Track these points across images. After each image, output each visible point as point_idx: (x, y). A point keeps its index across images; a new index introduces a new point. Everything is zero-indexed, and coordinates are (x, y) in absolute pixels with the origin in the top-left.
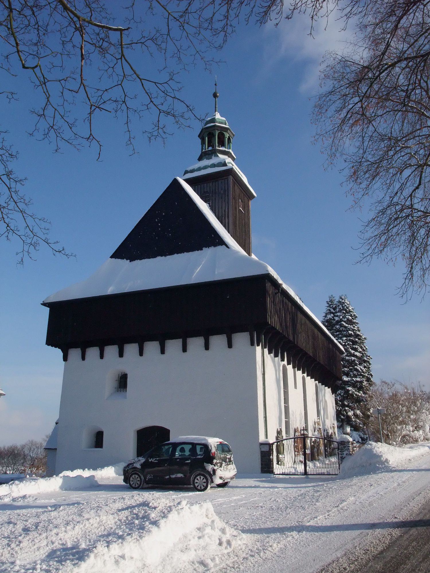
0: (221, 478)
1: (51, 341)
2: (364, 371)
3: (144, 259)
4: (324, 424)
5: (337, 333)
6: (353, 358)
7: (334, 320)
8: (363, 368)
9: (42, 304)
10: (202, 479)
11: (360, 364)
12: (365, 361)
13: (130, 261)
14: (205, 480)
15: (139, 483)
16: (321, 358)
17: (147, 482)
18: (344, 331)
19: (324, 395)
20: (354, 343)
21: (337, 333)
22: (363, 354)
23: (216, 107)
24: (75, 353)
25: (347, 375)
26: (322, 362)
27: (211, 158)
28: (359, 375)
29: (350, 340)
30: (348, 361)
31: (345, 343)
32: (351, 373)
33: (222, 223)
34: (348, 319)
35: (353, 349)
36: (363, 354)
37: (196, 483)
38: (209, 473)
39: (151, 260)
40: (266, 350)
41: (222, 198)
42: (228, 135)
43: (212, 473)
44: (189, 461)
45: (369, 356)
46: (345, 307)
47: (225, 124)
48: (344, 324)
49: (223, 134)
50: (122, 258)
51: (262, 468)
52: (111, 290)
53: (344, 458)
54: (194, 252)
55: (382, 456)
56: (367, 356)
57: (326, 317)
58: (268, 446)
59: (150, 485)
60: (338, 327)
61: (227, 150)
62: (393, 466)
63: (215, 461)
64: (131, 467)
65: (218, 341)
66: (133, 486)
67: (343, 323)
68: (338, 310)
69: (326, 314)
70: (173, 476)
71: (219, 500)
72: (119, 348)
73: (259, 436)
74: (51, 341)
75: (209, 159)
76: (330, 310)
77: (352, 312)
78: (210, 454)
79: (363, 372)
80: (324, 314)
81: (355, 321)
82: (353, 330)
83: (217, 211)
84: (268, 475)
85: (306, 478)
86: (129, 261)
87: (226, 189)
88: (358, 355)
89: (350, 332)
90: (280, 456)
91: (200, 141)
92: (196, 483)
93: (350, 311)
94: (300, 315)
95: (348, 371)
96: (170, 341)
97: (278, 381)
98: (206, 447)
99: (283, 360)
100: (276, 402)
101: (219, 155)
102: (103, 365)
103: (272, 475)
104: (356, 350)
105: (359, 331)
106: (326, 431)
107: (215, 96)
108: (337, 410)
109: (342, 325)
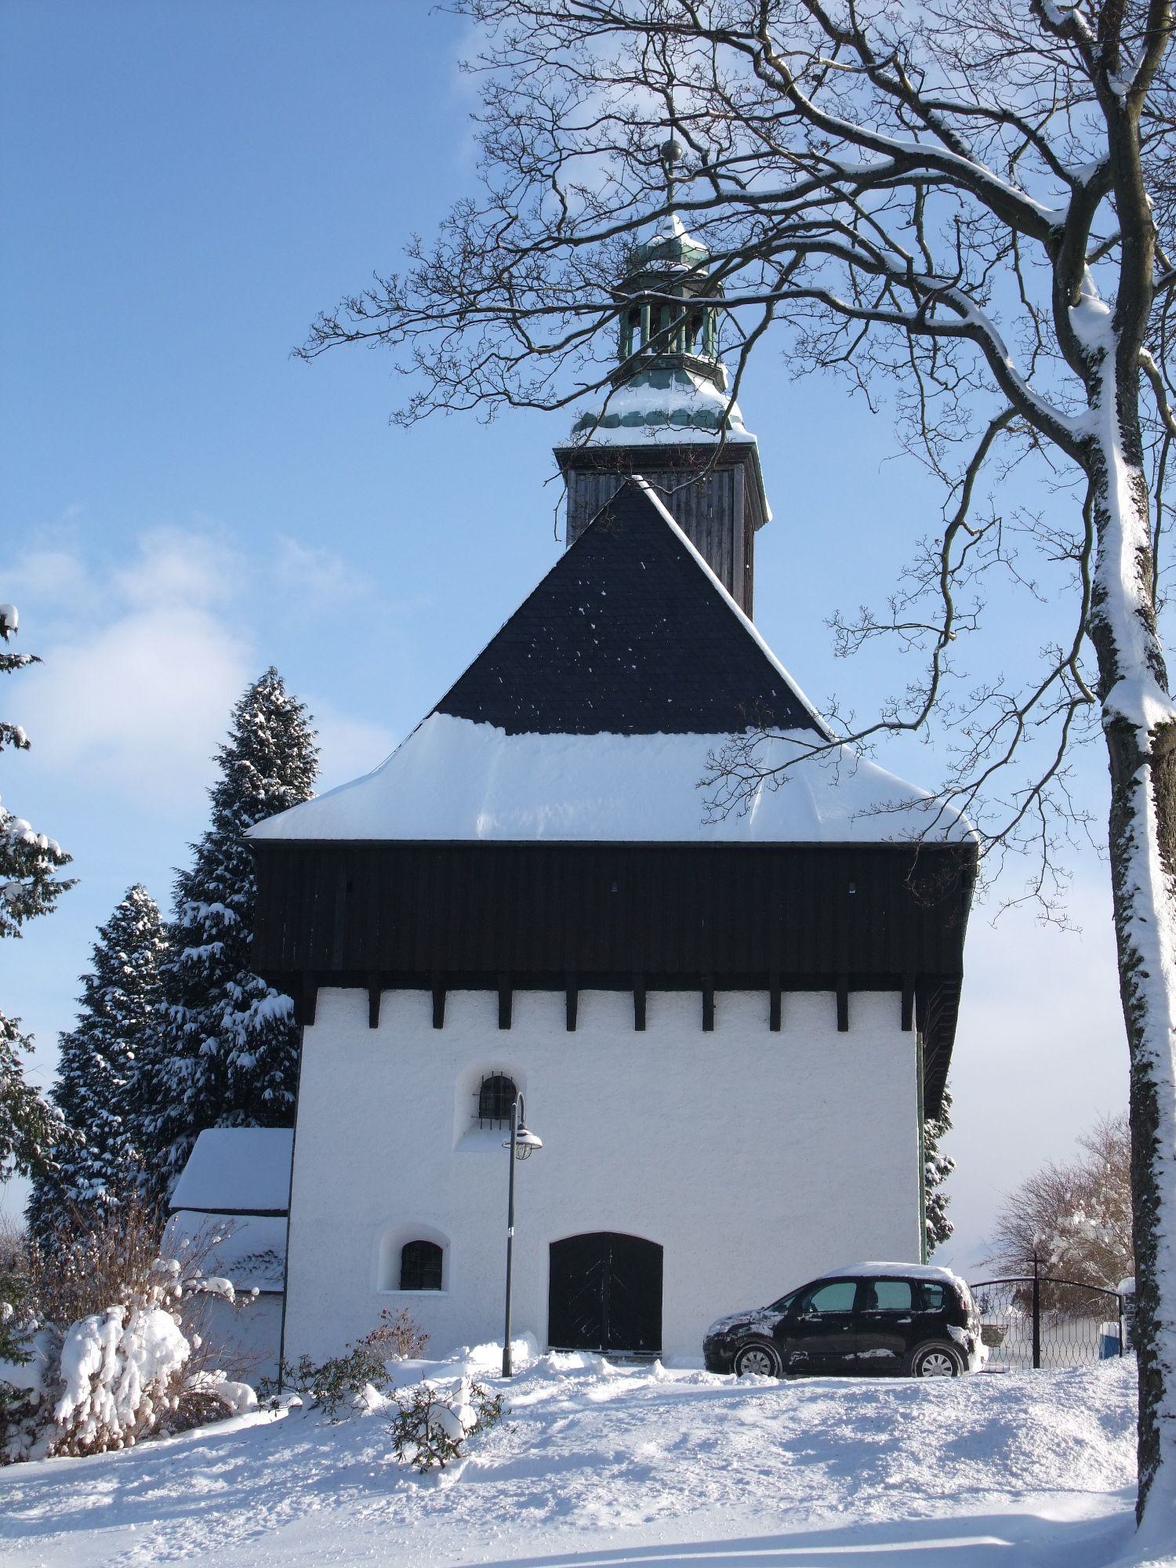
10: (940, 1361)
13: (508, 733)
38: (960, 1347)
39: (581, 739)
41: (709, 534)
44: (909, 1321)
64: (741, 1332)
72: (458, 988)
75: (660, 388)
87: (726, 505)
96: (663, 993)
98: (948, 1291)
101: (697, 381)
108: (295, 1090)
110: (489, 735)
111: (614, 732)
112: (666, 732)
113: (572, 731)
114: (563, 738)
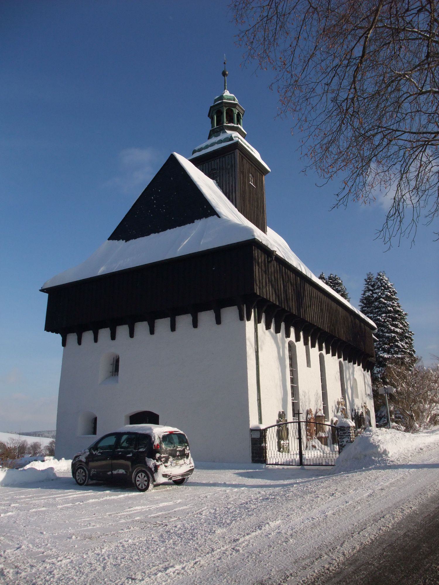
0: (165, 476)
1: (50, 327)
2: (406, 347)
3: (139, 237)
4: (352, 403)
5: (376, 310)
6: (393, 335)
7: (373, 297)
8: (404, 345)
9: (41, 290)
11: (401, 340)
12: (407, 337)
14: (146, 478)
15: (84, 478)
16: (342, 334)
17: (92, 478)
18: (383, 307)
19: (353, 374)
20: (394, 319)
21: (376, 310)
22: (403, 330)
23: (225, 85)
24: (72, 338)
25: (388, 352)
26: (344, 338)
27: (219, 135)
28: (400, 352)
29: (389, 317)
30: (388, 337)
31: (385, 319)
32: (392, 350)
33: (229, 198)
34: (387, 295)
35: (393, 325)
36: (403, 330)
37: (138, 481)
38: (150, 469)
40: (262, 326)
41: (229, 173)
42: (237, 111)
43: (153, 469)
44: (131, 455)
45: (411, 332)
46: (384, 284)
47: (234, 100)
48: (383, 300)
49: (232, 111)
50: (118, 239)
51: (253, 457)
52: (102, 271)
53: (344, 447)
54: (186, 225)
55: (379, 446)
56: (409, 332)
57: (364, 294)
58: (259, 433)
59: (94, 482)
60: (376, 303)
61: (235, 125)
62: (392, 459)
63: (158, 455)
65: (206, 318)
66: (79, 481)
67: (382, 299)
68: (376, 287)
69: (365, 292)
70: (115, 472)
71: (137, 508)
73: (249, 421)
74: (50, 327)
76: (368, 287)
77: (391, 288)
78: (152, 448)
79: (405, 348)
80: (363, 292)
81: (394, 297)
82: (392, 306)
83: (224, 186)
84: (259, 465)
85: (301, 469)
86: (124, 241)
87: (233, 163)
88: (398, 331)
89: (389, 308)
90: (282, 442)
91: (210, 120)
92: (138, 481)
93: (388, 287)
94: (307, 286)
95: (388, 348)
97: (281, 360)
99: (288, 335)
100: (279, 383)
102: (100, 348)
103: (264, 466)
104: (396, 326)
105: (399, 307)
106: (354, 411)
107: (224, 74)
109: (381, 302)
110: (122, 243)
111: (155, 233)
112: (170, 229)
113: (143, 236)
114: (141, 239)
